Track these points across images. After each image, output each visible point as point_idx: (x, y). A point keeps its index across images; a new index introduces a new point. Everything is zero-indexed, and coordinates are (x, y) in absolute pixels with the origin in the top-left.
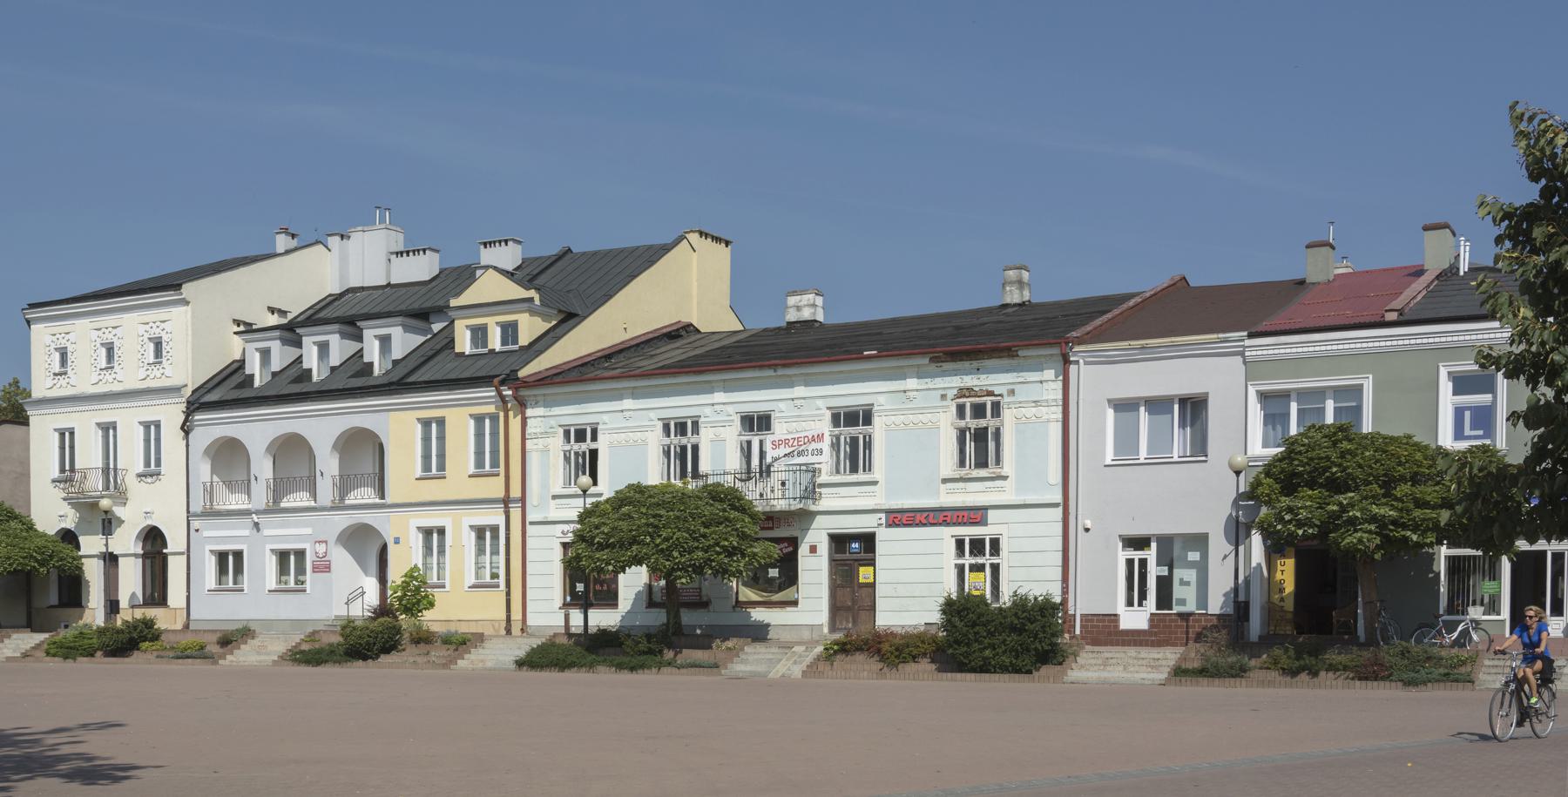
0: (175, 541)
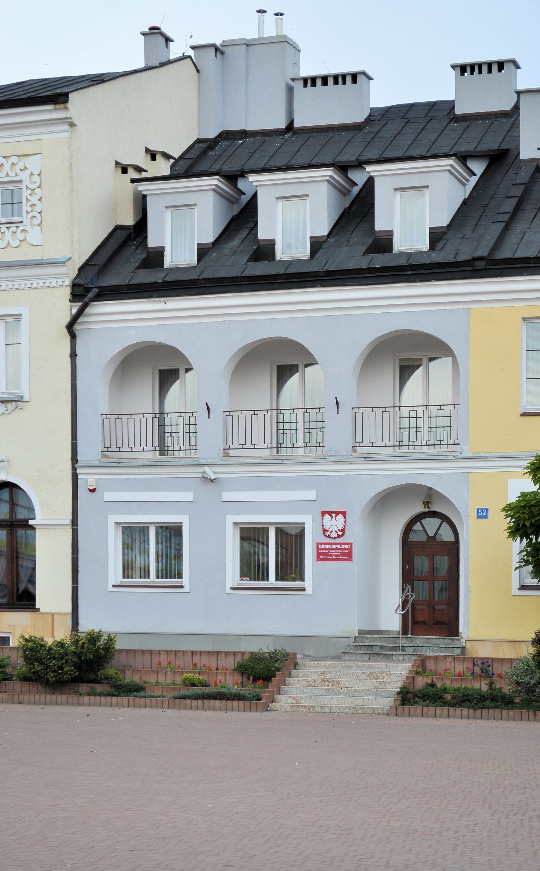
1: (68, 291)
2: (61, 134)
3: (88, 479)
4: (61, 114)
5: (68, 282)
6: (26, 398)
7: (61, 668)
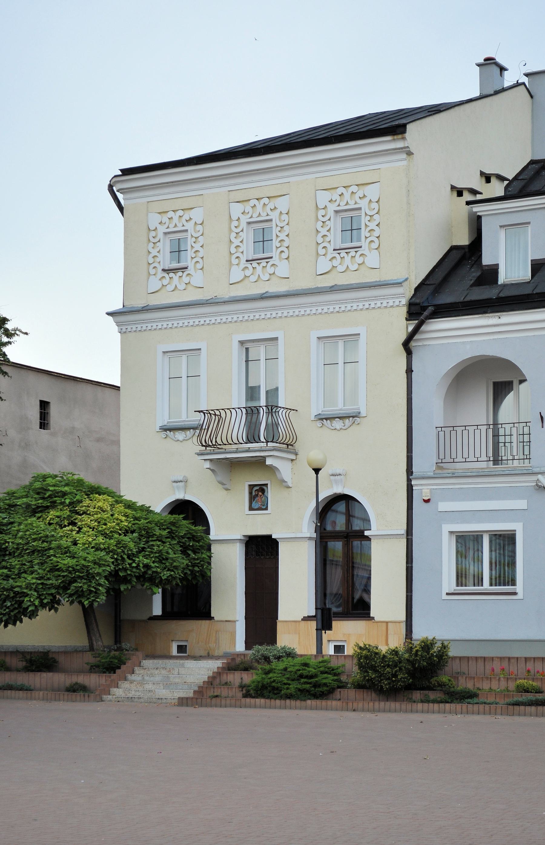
0: (383, 519)
1: (405, 310)
2: (399, 163)
3: (422, 489)
4: (400, 144)
5: (404, 301)
6: (363, 414)
7: (395, 675)
